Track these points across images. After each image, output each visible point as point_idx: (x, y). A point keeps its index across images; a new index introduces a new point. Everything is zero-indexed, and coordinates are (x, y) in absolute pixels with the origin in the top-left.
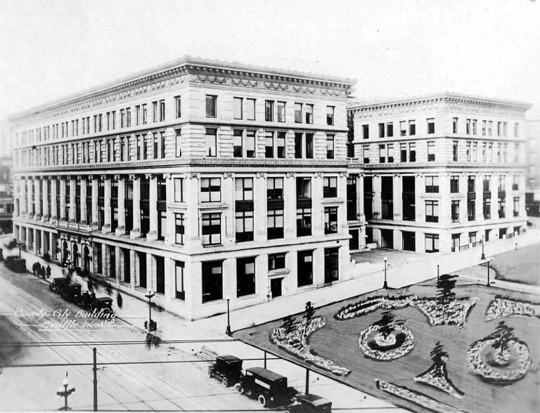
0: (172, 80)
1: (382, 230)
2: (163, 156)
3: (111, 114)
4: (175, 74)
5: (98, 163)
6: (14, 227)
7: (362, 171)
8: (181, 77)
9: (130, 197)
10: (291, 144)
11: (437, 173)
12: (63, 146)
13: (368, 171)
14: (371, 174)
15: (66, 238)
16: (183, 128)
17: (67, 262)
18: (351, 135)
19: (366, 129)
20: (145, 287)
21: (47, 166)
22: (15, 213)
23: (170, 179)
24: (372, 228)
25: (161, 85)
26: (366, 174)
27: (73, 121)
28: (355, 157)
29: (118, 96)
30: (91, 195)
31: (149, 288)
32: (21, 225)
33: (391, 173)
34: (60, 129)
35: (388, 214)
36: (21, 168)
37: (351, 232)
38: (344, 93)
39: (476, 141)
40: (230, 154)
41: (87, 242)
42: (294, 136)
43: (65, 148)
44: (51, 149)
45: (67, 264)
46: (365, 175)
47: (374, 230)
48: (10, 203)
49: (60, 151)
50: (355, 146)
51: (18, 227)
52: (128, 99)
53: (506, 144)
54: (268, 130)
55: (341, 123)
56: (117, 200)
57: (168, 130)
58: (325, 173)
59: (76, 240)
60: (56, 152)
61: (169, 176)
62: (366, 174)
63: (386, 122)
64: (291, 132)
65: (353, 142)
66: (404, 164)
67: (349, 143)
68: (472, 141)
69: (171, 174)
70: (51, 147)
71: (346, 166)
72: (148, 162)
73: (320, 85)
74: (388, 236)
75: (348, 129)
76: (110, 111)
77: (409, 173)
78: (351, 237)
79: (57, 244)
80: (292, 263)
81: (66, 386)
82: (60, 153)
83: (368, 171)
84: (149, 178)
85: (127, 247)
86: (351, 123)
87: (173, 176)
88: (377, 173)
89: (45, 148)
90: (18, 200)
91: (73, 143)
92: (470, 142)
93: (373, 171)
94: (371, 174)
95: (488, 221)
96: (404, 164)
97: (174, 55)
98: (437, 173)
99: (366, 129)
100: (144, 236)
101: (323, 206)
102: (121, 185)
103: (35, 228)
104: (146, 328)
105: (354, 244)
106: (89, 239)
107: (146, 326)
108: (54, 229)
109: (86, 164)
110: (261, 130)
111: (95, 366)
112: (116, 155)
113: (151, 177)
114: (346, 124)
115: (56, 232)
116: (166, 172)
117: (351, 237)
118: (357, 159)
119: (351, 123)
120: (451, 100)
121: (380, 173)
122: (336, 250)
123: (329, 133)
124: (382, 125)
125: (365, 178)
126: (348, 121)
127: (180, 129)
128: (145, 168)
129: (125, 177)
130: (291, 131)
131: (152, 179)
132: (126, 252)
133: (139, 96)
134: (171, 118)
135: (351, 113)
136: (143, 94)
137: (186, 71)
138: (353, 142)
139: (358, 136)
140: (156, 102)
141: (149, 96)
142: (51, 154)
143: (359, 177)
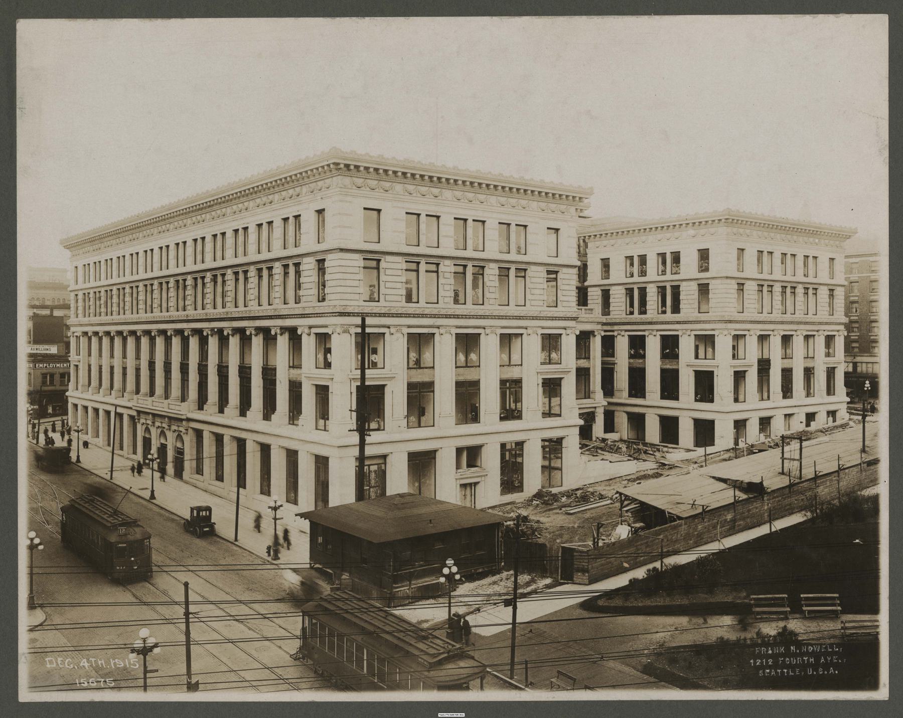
0: (284, 193)
1: (628, 413)
2: (297, 301)
3: (265, 226)
4: (281, 187)
5: (241, 308)
6: (70, 406)
7: (599, 327)
8: (326, 181)
9: (271, 363)
10: (492, 284)
11: (713, 330)
12: (132, 287)
13: (608, 328)
14: (613, 331)
15: (149, 422)
16: (329, 257)
17: (150, 457)
18: (583, 272)
19: (606, 264)
20: (269, 495)
21: (200, 311)
22: (71, 385)
23: (309, 335)
24: (614, 411)
25: (295, 194)
26: (605, 331)
27: (236, 231)
28: (589, 307)
29: (229, 210)
30: (188, 360)
31: (274, 497)
32: (80, 403)
33: (644, 331)
34: (128, 263)
35: (637, 385)
36: (82, 319)
37: (581, 415)
38: (573, 209)
39: (771, 283)
40: (399, 298)
41: (181, 429)
42: (497, 272)
43: (149, 288)
44: (128, 290)
45: (150, 460)
46: (603, 334)
47: (616, 414)
48: (66, 370)
49: (140, 294)
50: (589, 289)
51: (76, 406)
52: (244, 214)
53: (816, 289)
54: (459, 262)
55: (569, 256)
56: (188, 364)
57: (306, 260)
58: (543, 328)
59: (149, 422)
60: (121, 297)
61: (307, 331)
62: (605, 331)
63: (636, 253)
64: (494, 266)
65: (586, 284)
66: (663, 318)
67: (580, 285)
68: (766, 283)
69: (310, 327)
70: (127, 286)
71: (575, 319)
72: (250, 311)
73: (551, 199)
74: (637, 421)
75: (579, 263)
76: (198, 238)
77: (670, 330)
78: (582, 422)
79: (668, 552)
80: (491, 460)
81: (144, 640)
82: (142, 297)
83: (608, 328)
84: (251, 334)
85: (243, 435)
86: (582, 255)
87: (314, 330)
88: (686, 330)
89: (146, 286)
90: (77, 366)
91: (236, 270)
92: (762, 286)
93: (616, 328)
94: (613, 331)
95: (788, 402)
96: (663, 318)
97: (313, 148)
98: (713, 330)
99: (606, 264)
100: (243, 413)
101: (541, 377)
102: (213, 344)
103: (90, 405)
104: (269, 555)
105: (585, 432)
106: (184, 423)
107: (269, 552)
108: (131, 408)
109: (165, 314)
110: (447, 262)
111: (187, 608)
112: (227, 299)
113: (278, 331)
114: (575, 255)
115: (135, 413)
116: (300, 324)
117: (582, 422)
118: (592, 310)
119: (582, 255)
120: (732, 221)
121: (657, 330)
122: (559, 441)
123: (551, 268)
124: (663, 256)
125: (603, 338)
126: (579, 253)
127: (324, 260)
128: (137, 323)
129: (241, 331)
130: (492, 265)
131: (281, 334)
132: (219, 438)
133: (162, 235)
134: (308, 243)
135: (584, 241)
136: (268, 207)
137: (334, 172)
138: (586, 284)
139: (594, 276)
140: (288, 218)
141: (277, 210)
142: (128, 299)
143: (595, 336)
